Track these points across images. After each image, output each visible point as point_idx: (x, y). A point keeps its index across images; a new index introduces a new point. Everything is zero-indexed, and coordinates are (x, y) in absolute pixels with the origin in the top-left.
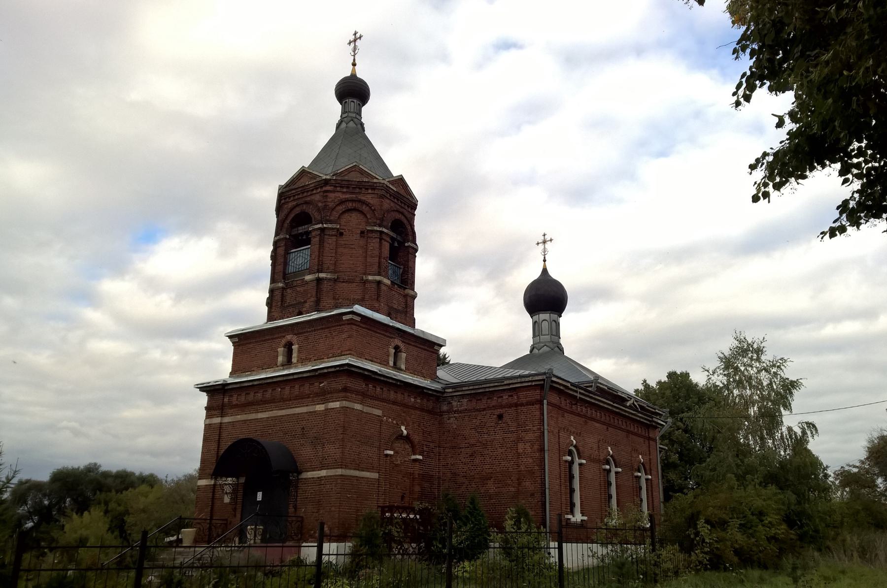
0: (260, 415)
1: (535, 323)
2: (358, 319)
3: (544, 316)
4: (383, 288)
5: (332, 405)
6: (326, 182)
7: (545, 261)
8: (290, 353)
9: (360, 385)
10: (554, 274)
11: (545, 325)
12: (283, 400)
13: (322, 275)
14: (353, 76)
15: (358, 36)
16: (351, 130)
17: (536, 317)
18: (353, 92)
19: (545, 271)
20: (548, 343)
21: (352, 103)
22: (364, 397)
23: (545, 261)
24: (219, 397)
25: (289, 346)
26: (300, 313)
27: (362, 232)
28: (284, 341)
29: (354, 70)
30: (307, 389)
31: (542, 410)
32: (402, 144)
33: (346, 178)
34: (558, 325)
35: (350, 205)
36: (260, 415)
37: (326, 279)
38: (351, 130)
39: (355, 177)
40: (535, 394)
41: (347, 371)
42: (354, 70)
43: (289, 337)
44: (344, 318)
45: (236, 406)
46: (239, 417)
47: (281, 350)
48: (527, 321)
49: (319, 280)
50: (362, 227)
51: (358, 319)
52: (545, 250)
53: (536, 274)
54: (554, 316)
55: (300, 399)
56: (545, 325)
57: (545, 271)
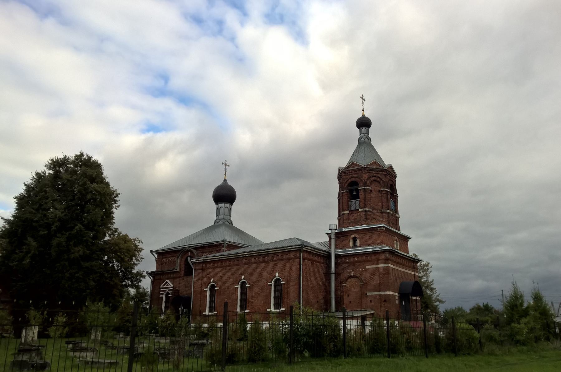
2: (384, 229)
5: (381, 266)
10: (230, 183)
13: (368, 209)
14: (363, 115)
16: (365, 143)
19: (225, 180)
20: (223, 221)
21: (363, 129)
22: (397, 263)
24: (157, 277)
25: (355, 240)
27: (379, 191)
29: (363, 113)
31: (300, 261)
32: (388, 153)
35: (372, 179)
37: (368, 211)
39: (375, 167)
40: (296, 254)
42: (363, 113)
44: (379, 229)
47: (351, 241)
48: (214, 206)
49: (366, 211)
50: (378, 188)
51: (384, 229)
53: (220, 182)
54: (228, 205)
57: (225, 180)
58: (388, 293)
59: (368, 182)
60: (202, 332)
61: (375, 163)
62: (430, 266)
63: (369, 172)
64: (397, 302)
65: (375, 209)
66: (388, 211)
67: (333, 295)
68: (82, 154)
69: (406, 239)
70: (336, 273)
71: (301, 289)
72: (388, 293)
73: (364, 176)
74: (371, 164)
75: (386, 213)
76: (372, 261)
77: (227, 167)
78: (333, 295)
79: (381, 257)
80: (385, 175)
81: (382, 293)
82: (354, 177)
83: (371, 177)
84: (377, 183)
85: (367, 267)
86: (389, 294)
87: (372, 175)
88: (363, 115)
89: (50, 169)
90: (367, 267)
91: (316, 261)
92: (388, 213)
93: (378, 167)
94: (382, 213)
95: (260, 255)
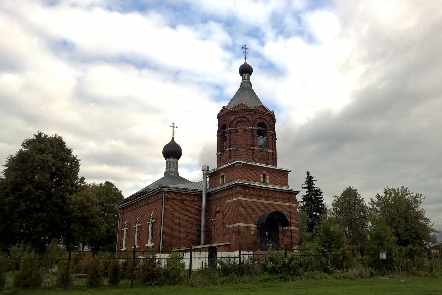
0: (263, 201)
1: (167, 163)
2: (241, 165)
3: (172, 159)
4: (256, 151)
6: (252, 110)
7: (173, 135)
8: (264, 178)
9: (277, 195)
10: (177, 141)
11: (172, 163)
12: (272, 198)
13: (231, 148)
14: (246, 63)
15: (244, 47)
16: (246, 88)
17: (168, 160)
18: (308, 173)
19: (173, 139)
21: (246, 76)
22: (246, 195)
23: (173, 135)
26: (267, 164)
27: (245, 130)
28: (262, 173)
29: (245, 61)
30: (281, 196)
33: (238, 109)
34: (177, 163)
36: (263, 201)
37: (232, 150)
38: (246, 88)
39: (242, 108)
41: (237, 185)
42: (245, 61)
43: (265, 172)
44: (236, 165)
45: (253, 195)
46: (254, 200)
47: (262, 176)
48: (163, 161)
49: (230, 150)
50: (244, 128)
51: (241, 165)
52: (173, 131)
53: (169, 141)
54: (176, 160)
55: (279, 199)
56: (172, 163)
57: (173, 139)
58: (237, 224)
59: (234, 123)
60: (154, 265)
61: (242, 104)
62: (422, 197)
63: (235, 113)
64: (253, 233)
65: (240, 148)
66: (252, 148)
67: (202, 229)
68: (40, 134)
69: (284, 173)
70: (206, 210)
71: (162, 226)
72: (237, 224)
73: (230, 118)
74: (237, 107)
75: (250, 149)
76: (229, 195)
77: (175, 129)
78: (202, 229)
79: (234, 191)
80: (252, 115)
81: (234, 225)
82: (266, 120)
83: (237, 118)
84: (243, 123)
85: (227, 201)
86: (239, 226)
87: (238, 116)
88: (246, 63)
89: (26, 147)
90: (227, 201)
91: (186, 200)
92: (253, 149)
93: (244, 108)
94: (247, 150)
95: (146, 198)
